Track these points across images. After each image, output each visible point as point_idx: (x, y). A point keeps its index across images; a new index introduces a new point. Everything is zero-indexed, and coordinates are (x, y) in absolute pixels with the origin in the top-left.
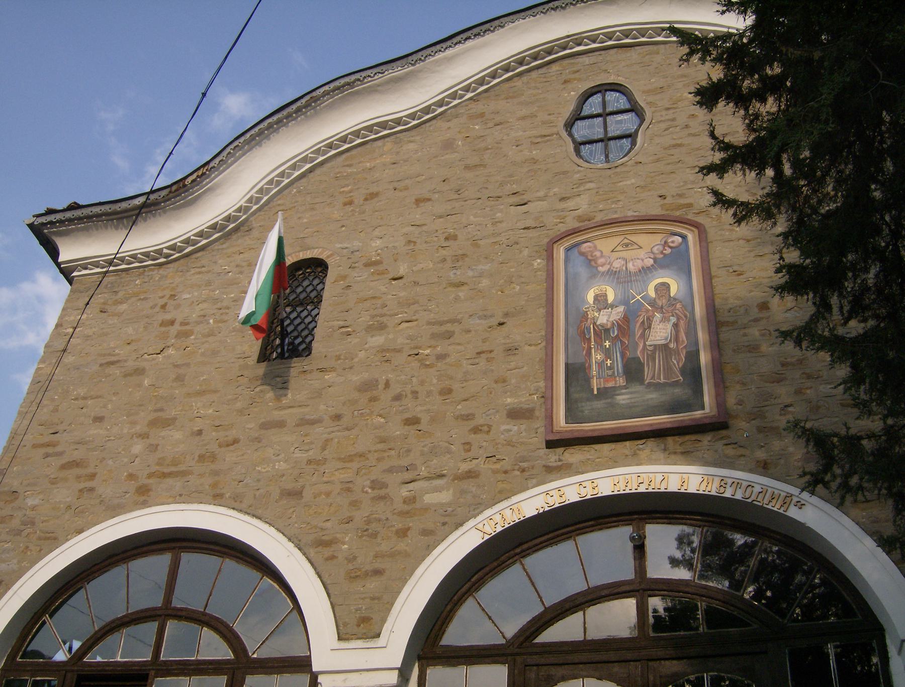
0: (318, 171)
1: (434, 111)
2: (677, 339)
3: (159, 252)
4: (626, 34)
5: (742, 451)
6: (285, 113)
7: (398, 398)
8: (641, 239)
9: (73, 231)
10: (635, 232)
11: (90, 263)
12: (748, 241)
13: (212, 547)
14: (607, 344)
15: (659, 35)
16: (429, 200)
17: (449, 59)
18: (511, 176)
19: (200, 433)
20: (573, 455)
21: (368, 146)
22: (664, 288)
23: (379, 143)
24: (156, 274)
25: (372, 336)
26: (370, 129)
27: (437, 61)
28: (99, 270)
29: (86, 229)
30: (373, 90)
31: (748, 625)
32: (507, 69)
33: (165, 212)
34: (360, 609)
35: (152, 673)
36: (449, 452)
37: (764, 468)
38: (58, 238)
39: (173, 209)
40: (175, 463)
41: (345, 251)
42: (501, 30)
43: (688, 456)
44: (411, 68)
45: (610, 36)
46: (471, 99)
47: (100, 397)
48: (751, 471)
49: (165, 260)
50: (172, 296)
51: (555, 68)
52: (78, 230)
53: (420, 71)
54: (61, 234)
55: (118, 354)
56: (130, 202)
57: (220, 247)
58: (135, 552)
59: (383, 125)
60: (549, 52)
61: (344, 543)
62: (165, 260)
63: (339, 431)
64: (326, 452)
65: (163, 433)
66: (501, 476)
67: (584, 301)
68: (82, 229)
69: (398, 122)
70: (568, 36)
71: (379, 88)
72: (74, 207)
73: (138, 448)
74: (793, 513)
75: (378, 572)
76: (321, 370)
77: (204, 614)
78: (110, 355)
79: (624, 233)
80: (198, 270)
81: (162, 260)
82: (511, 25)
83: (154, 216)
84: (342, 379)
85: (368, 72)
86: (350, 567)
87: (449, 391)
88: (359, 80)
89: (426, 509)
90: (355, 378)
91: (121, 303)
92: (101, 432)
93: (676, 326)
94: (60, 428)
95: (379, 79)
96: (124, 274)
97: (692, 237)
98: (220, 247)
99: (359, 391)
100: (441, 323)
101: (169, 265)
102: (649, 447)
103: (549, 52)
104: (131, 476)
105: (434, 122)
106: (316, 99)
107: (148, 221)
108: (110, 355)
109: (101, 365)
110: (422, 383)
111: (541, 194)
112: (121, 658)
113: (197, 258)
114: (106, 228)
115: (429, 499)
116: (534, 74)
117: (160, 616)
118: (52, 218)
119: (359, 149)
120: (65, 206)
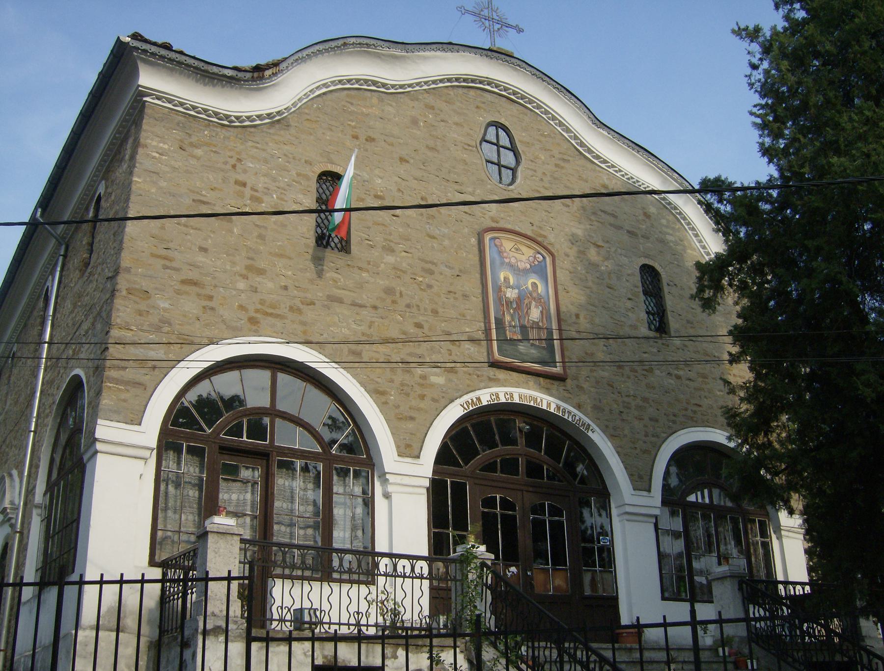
0: (329, 96)
1: (406, 88)
2: (542, 321)
3: (227, 117)
4: (515, 93)
5: (570, 395)
6: (327, 45)
7: (408, 306)
8: (524, 249)
9: (159, 65)
10: (521, 243)
11: (164, 97)
12: (570, 273)
13: (299, 374)
14: (512, 311)
15: (560, 126)
16: (408, 162)
17: (425, 58)
18: (454, 168)
19: (286, 288)
20: (501, 374)
21: (361, 92)
22: (534, 285)
23: (368, 94)
24: (223, 133)
25: (387, 255)
26: (366, 81)
27: (419, 56)
28: (170, 106)
29: (172, 70)
30: (378, 56)
31: (562, 482)
32: (449, 80)
33: (241, 88)
34: (405, 439)
35: (275, 453)
36: (440, 352)
37: (579, 407)
38: (142, 64)
39: (248, 89)
40: (273, 306)
41: (359, 177)
42: (457, 53)
43: (548, 391)
44: (406, 54)
45: (506, 89)
46: (425, 90)
47: (199, 229)
48: (574, 407)
49: (228, 123)
50: (239, 160)
51: (472, 93)
52: (164, 67)
53: (408, 58)
54: (145, 61)
55: (205, 196)
56: (221, 69)
57: (268, 131)
58: (245, 364)
59: (375, 83)
60: (473, 81)
61: (392, 395)
62: (228, 123)
63: (377, 317)
64: (372, 330)
65: (258, 279)
66: (468, 376)
67: (499, 278)
68: (168, 68)
69: (384, 85)
70: (487, 78)
71: (383, 57)
72: (167, 47)
73: (241, 285)
74: (590, 434)
75: (412, 418)
76: (360, 268)
77: (298, 418)
78: (198, 193)
79: (516, 242)
80: (254, 144)
81: (226, 123)
82: (463, 54)
83: (232, 87)
84: (372, 280)
85: (380, 43)
86: (397, 411)
87: (437, 312)
88: (374, 45)
89: (432, 385)
90: (382, 282)
91: (197, 147)
92: (208, 261)
93: (542, 312)
94: (171, 245)
95: (386, 51)
96: (191, 119)
97: (548, 260)
98: (268, 131)
99: (385, 293)
100: (427, 262)
101: (229, 129)
102: (531, 380)
103: (473, 81)
104: (242, 307)
105: (402, 96)
106: (345, 44)
107: (225, 88)
108: (198, 193)
109: (194, 200)
110: (421, 300)
111: (470, 189)
112: (210, 429)
113: (251, 132)
114: (189, 77)
115: (434, 379)
116: (460, 91)
117: (271, 414)
118: (163, 52)
119: (356, 91)
120: (160, 42)
